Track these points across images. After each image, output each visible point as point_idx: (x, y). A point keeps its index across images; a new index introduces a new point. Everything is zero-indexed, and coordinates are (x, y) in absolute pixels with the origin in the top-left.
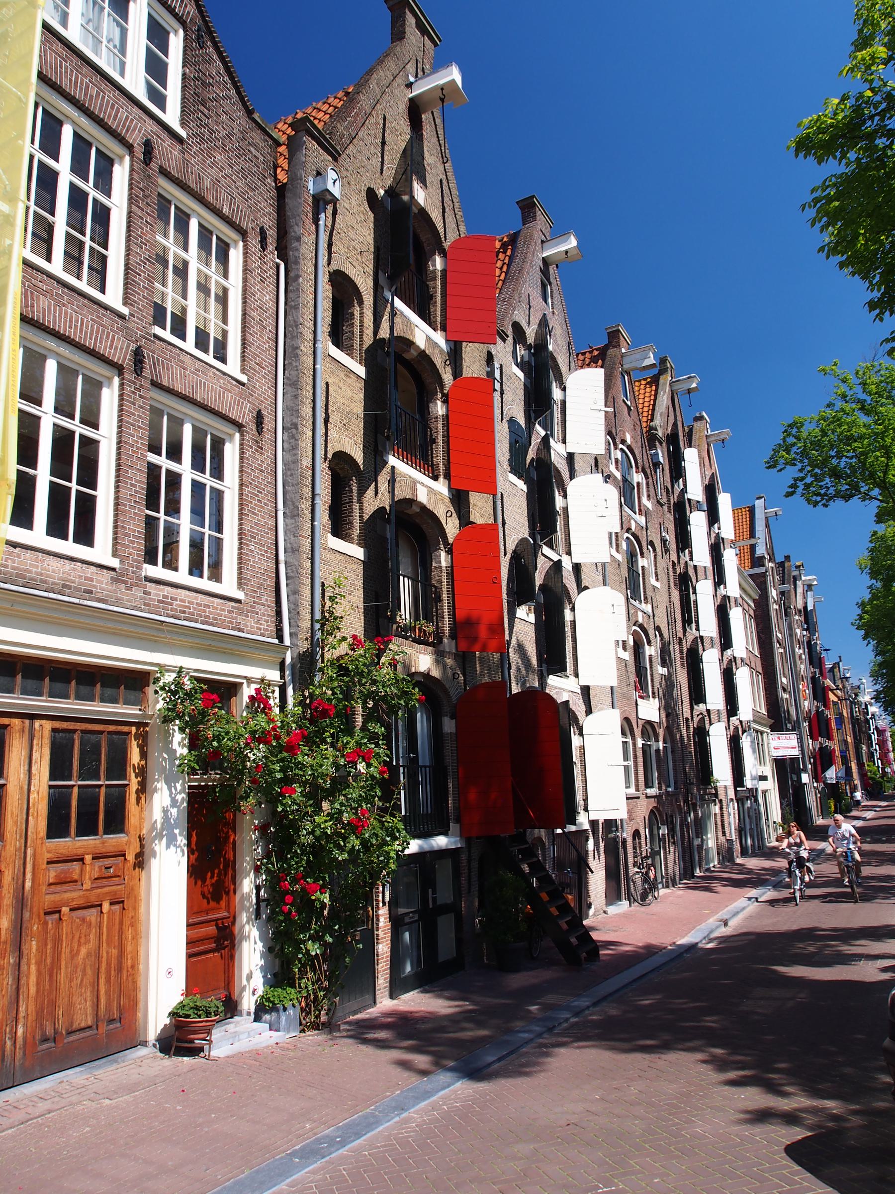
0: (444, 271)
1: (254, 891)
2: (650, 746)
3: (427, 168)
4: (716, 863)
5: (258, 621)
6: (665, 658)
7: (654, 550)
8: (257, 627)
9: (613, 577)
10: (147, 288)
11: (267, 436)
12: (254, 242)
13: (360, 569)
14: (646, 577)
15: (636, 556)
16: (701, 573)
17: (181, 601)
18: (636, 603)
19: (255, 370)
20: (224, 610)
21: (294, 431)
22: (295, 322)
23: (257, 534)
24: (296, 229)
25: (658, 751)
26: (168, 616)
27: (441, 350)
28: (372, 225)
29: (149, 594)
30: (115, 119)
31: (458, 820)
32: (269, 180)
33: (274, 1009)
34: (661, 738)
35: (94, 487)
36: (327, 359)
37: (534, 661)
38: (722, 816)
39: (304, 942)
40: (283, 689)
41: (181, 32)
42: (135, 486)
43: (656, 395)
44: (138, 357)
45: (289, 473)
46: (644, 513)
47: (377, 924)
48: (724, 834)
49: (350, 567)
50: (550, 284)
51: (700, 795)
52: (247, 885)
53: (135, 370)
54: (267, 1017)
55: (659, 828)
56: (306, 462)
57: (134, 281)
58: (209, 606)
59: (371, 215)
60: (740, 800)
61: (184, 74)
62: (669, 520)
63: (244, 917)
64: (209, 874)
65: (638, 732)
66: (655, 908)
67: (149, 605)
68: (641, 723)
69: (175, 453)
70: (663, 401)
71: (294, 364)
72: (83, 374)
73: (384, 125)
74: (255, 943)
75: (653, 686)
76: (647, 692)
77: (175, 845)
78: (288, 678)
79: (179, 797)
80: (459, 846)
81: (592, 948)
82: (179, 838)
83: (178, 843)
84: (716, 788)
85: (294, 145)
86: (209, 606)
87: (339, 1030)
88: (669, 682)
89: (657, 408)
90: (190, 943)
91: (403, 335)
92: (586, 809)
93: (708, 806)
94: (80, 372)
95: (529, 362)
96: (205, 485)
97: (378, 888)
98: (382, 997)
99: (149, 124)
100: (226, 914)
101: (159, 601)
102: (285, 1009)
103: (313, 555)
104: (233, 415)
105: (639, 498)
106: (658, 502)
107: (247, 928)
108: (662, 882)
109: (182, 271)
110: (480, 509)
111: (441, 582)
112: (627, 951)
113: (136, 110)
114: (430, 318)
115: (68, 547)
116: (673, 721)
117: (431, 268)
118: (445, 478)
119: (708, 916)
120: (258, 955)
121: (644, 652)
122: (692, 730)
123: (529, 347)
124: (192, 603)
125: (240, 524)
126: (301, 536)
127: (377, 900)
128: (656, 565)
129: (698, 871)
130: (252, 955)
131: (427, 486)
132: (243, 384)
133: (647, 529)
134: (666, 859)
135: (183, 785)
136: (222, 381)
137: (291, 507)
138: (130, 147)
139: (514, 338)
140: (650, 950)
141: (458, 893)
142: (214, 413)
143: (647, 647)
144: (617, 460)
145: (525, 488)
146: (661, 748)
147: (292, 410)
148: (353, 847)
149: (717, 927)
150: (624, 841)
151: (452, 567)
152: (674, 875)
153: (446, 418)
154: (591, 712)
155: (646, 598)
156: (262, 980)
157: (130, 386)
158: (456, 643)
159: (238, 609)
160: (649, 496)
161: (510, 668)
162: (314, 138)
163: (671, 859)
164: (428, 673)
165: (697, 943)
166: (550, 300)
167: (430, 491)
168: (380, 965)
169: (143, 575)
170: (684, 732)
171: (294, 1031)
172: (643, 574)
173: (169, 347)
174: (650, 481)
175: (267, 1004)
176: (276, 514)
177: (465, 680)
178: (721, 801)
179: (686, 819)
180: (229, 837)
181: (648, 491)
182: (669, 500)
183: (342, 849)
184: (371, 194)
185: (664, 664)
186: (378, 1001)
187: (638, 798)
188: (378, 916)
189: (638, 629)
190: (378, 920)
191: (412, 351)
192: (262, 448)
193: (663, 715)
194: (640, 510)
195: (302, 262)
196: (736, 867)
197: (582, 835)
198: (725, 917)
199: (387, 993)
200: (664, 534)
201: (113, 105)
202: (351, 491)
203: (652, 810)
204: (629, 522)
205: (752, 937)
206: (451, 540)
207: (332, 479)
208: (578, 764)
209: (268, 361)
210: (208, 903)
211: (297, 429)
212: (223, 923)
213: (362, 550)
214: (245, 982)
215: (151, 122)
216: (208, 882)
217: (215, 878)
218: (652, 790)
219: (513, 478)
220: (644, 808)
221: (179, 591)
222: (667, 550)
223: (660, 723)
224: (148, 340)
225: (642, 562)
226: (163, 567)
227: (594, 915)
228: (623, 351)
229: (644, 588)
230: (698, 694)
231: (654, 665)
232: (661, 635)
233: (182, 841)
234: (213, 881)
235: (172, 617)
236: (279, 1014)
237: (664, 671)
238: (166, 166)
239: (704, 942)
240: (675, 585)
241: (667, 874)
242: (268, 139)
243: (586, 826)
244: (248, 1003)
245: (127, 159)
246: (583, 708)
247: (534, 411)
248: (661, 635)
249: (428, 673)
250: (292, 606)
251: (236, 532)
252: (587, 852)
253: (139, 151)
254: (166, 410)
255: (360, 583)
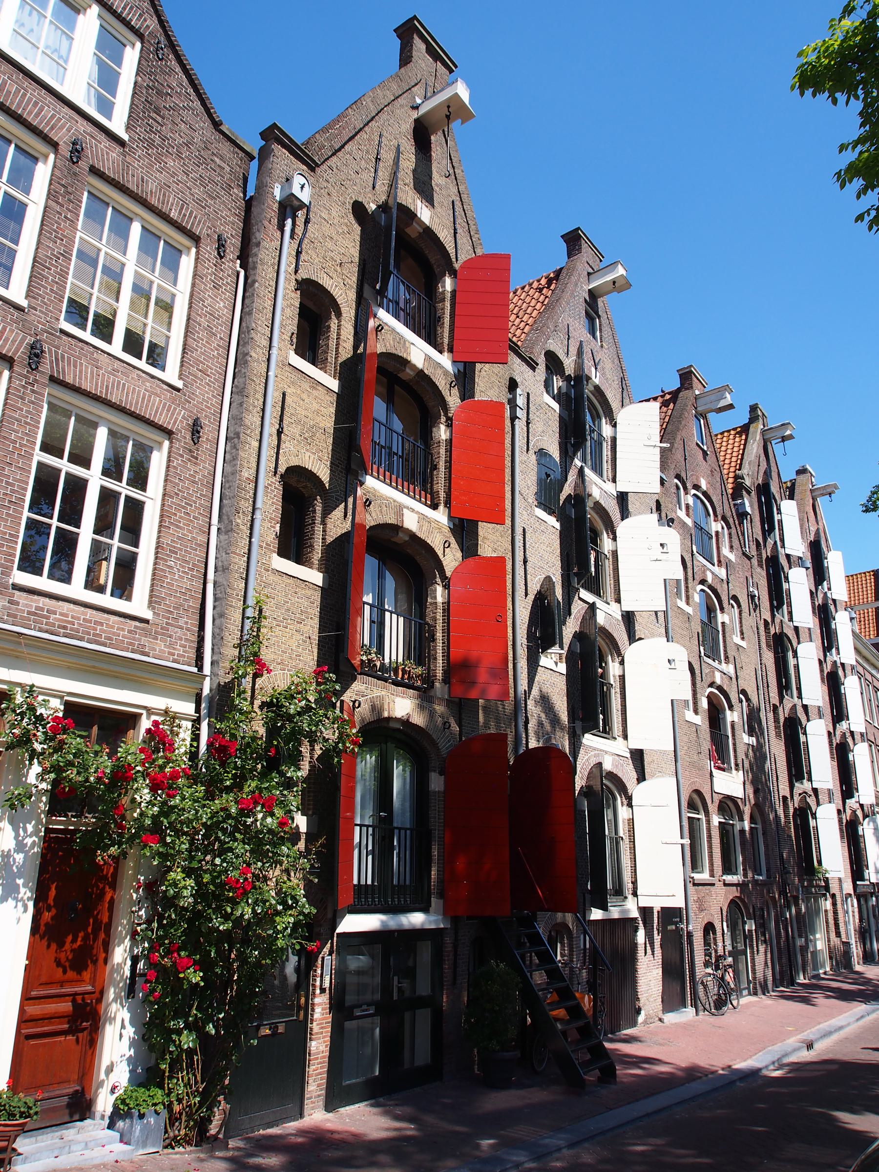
0: (454, 293)
1: (129, 963)
2: (733, 825)
3: (435, 188)
4: (828, 969)
5: (171, 645)
6: (753, 724)
7: (739, 606)
8: (168, 652)
9: (680, 631)
10: (57, 283)
11: (205, 445)
12: (209, 249)
13: (317, 596)
14: (727, 635)
15: (715, 611)
16: (803, 635)
17: (61, 614)
18: (715, 664)
19: (196, 377)
20: (123, 630)
21: (236, 440)
22: (248, 327)
23: (181, 550)
24: (257, 234)
25: (742, 831)
26: (40, 630)
27: (446, 372)
28: (358, 238)
29: (18, 604)
30: (37, 115)
31: (441, 895)
32: (235, 190)
33: (128, 1115)
34: (747, 817)
35: (136, 544)
36: (287, 368)
37: (564, 717)
38: (835, 913)
39: (179, 1032)
40: (197, 722)
41: (138, 45)
42: (13, 485)
43: (745, 445)
44: (35, 354)
45: (227, 485)
46: (724, 565)
47: (312, 1015)
48: (838, 934)
49: (301, 592)
50: (599, 317)
51: (803, 886)
52: (120, 954)
53: (29, 364)
54: (120, 1124)
55: (744, 923)
56: (248, 473)
57: (40, 274)
58: (102, 624)
59: (357, 229)
60: (861, 897)
61: (136, 83)
62: (761, 576)
63: (111, 994)
64: (70, 938)
65: (713, 808)
66: (729, 1017)
67: (15, 616)
68: (717, 798)
69: (82, 459)
70: (752, 449)
71: (243, 371)
72: (134, 440)
73: (380, 142)
74: (123, 1026)
75: (736, 757)
76: (729, 763)
77: (17, 900)
78: (204, 712)
79: (29, 841)
80: (442, 926)
81: (607, 1065)
82: (22, 890)
83: (20, 896)
84: (827, 880)
85: (264, 154)
86: (102, 624)
87: (227, 1148)
88: (759, 755)
89: (745, 457)
90: (24, 1020)
91: (394, 351)
92: (635, 894)
93: (816, 901)
94: (74, 414)
95: (567, 394)
96: (120, 494)
97: (315, 971)
98: (313, 1108)
99: (82, 125)
100: (89, 988)
101: (29, 613)
102: (142, 1116)
103: (247, 575)
104: (160, 420)
105: (718, 548)
106: (744, 554)
107: (114, 1007)
108: (748, 988)
109: (114, 275)
110: (491, 540)
111: (435, 619)
112: (662, 1073)
113: (66, 110)
114: (436, 340)
115: (106, 600)
116: (765, 798)
117: (441, 290)
118: (445, 506)
119: (790, 1034)
120: (126, 1042)
121: (724, 718)
122: (791, 810)
123: (568, 379)
124: (79, 619)
125: (159, 537)
126: (235, 553)
127: (314, 985)
128: (741, 622)
129: (802, 977)
130: (117, 1045)
131: (418, 513)
132: (178, 390)
133: (728, 583)
134: (753, 960)
135: (36, 827)
136: (148, 384)
137: (226, 522)
138: (55, 145)
139: (547, 367)
140: (693, 1073)
141: (437, 984)
142: (126, 413)
143: (728, 712)
144: (687, 506)
145: (558, 525)
146: (747, 828)
147: (236, 419)
148: (242, 915)
149: (795, 1050)
150: (690, 935)
151: (449, 602)
152: (765, 981)
153: (450, 442)
154: (645, 780)
155: (727, 658)
156: (128, 1075)
157: (21, 380)
158: (449, 687)
159: (143, 629)
160: (731, 547)
161: (527, 722)
162: (284, 146)
163: (761, 961)
164: (408, 720)
165: (760, 1070)
166: (598, 333)
167: (423, 519)
168: (312, 1068)
169: (11, 582)
170: (781, 812)
171: (154, 1146)
172: (724, 631)
173: (80, 344)
174: (733, 531)
175: (121, 1107)
176: (209, 529)
177: (460, 731)
178: (833, 896)
179: (783, 914)
180: (104, 894)
181: (731, 541)
182: (760, 555)
183: (226, 917)
184: (358, 209)
185: (751, 732)
186: (306, 1112)
187: (713, 885)
188: (313, 1004)
189: (716, 691)
190: (313, 1010)
191: (408, 370)
192: (197, 458)
193: (750, 791)
194: (719, 561)
195: (259, 266)
196: (852, 976)
197: (627, 925)
198: (812, 1037)
199: (321, 1103)
200: (751, 589)
201: (36, 104)
202: (314, 511)
203: (732, 901)
204: (704, 572)
205: (834, 1067)
206: (448, 574)
207: (283, 495)
208: (627, 840)
209: (214, 368)
210: (65, 972)
211: (239, 438)
212: (83, 999)
213: (321, 575)
214: (103, 1076)
215: (85, 123)
216: (67, 946)
217: (79, 943)
218: (735, 877)
219: (540, 513)
220: (719, 899)
221: (61, 603)
222: (756, 607)
223: (744, 801)
224: (53, 335)
225: (721, 618)
226: (48, 578)
227: (645, 1022)
228: (697, 392)
229: (725, 647)
230: (798, 767)
231: (737, 733)
232: (748, 700)
233: (26, 893)
234: (75, 946)
235: (47, 632)
236: (132, 1122)
237: (753, 741)
238: (100, 166)
239: (772, 1067)
240: (768, 646)
241: (755, 978)
242: (239, 151)
243: (635, 914)
244: (104, 1103)
245: (52, 157)
246: (634, 775)
247: (573, 446)
248: (748, 700)
249: (408, 720)
250: (217, 631)
251: (154, 545)
252: (635, 946)
253: (65, 150)
254: (75, 411)
255: (316, 611)
